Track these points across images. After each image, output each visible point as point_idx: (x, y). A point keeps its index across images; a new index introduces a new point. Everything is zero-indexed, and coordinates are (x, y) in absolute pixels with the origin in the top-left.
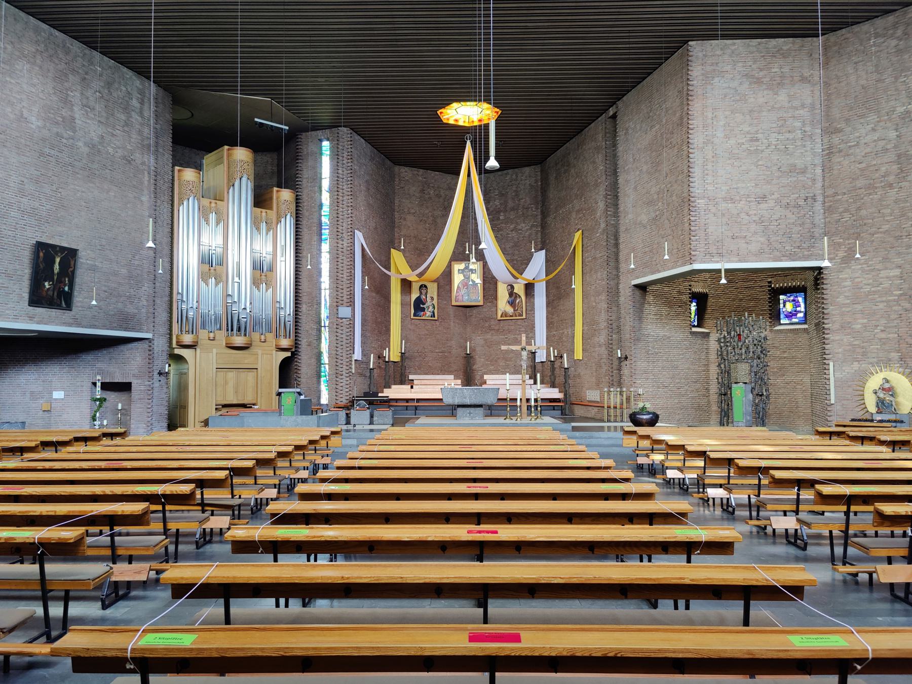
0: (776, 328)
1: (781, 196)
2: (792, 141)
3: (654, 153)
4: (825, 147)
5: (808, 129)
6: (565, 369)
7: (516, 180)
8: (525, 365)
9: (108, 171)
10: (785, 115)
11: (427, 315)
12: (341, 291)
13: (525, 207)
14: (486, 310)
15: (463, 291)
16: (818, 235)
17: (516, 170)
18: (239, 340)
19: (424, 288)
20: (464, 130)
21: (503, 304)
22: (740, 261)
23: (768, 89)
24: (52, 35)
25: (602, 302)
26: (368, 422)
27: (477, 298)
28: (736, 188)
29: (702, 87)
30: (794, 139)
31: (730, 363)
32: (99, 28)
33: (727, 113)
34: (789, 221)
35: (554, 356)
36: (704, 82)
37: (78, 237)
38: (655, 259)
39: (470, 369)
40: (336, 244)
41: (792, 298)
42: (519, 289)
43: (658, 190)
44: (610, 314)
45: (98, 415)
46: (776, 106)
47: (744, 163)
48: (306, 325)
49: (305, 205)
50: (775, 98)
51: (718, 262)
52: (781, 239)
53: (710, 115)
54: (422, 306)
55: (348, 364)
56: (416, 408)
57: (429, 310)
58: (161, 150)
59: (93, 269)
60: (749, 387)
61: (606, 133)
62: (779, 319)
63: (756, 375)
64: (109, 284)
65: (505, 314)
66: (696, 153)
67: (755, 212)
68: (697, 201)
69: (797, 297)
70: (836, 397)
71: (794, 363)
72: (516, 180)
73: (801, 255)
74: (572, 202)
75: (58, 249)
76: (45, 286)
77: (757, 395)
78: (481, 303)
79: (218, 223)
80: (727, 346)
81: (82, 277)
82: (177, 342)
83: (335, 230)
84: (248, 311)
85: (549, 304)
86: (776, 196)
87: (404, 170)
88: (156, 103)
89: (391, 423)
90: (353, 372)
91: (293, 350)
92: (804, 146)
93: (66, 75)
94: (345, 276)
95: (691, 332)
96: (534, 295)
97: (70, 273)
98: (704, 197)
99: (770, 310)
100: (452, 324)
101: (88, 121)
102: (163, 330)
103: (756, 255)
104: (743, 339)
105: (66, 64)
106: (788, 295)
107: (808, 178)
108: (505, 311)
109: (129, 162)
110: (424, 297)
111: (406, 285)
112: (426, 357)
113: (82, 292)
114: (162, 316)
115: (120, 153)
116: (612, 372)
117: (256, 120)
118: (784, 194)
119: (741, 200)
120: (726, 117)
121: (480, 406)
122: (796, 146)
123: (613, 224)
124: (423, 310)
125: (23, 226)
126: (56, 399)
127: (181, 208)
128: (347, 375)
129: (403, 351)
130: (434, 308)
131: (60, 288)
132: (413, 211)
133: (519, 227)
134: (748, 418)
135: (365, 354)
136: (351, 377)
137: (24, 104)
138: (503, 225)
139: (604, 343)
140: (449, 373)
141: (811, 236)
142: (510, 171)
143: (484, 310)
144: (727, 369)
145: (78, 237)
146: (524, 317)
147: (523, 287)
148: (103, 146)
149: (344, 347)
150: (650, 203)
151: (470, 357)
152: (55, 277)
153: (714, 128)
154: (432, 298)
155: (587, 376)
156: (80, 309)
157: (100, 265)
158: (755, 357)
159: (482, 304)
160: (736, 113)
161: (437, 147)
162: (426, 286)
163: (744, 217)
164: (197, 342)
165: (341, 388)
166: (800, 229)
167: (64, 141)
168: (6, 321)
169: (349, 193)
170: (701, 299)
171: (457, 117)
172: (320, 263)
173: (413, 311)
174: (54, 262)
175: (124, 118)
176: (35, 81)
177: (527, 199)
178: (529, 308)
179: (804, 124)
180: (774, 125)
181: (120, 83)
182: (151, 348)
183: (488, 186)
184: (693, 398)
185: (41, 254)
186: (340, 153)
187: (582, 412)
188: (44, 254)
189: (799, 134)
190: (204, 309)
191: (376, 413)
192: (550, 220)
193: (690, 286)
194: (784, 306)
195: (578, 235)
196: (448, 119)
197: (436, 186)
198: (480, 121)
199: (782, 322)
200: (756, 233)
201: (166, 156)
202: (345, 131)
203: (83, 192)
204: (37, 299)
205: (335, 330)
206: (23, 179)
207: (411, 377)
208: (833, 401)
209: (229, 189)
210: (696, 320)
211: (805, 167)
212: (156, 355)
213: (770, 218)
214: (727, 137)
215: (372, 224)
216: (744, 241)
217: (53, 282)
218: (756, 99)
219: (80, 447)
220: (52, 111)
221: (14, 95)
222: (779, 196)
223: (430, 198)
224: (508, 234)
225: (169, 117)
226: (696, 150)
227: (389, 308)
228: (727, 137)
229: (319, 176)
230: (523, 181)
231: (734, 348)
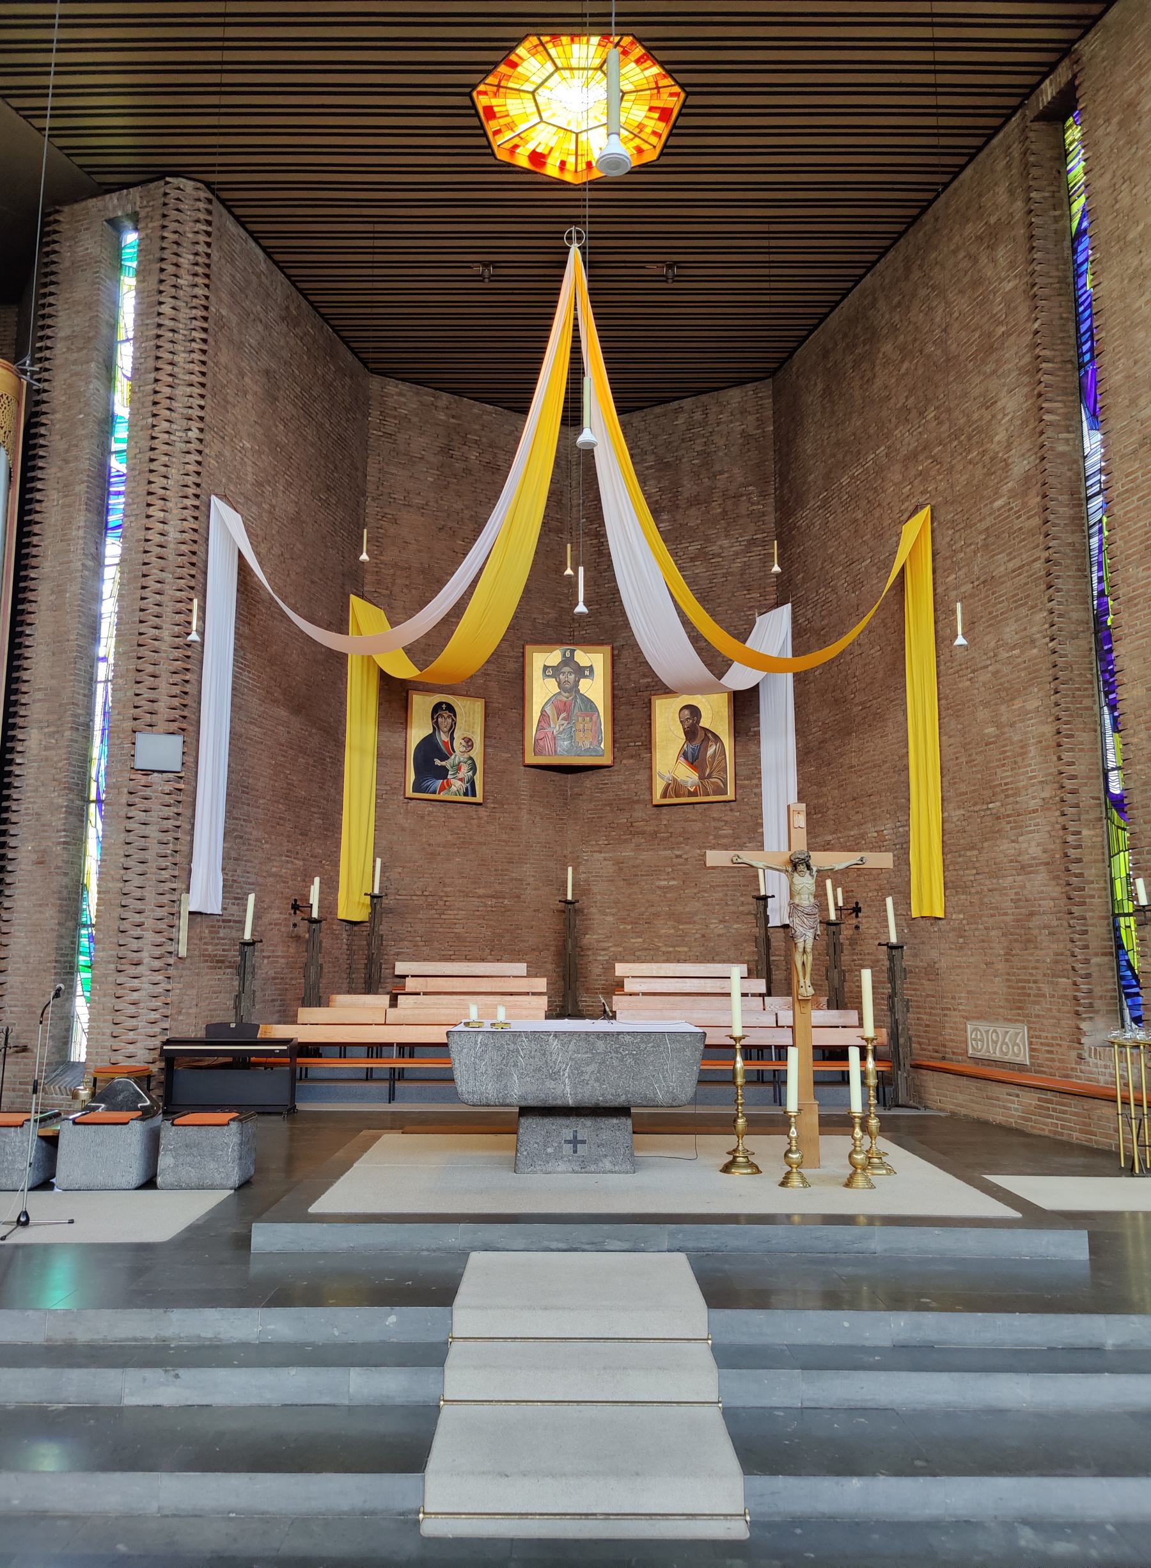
6: (892, 947)
7: (704, 423)
8: (810, 934)
11: (454, 788)
13: (731, 493)
14: (620, 778)
17: (704, 398)
19: (446, 714)
26: (135, 1175)
35: (838, 909)
39: (575, 946)
40: (141, 535)
54: (438, 762)
55: (162, 925)
56: (396, 1076)
57: (460, 775)
61: (1026, 166)
65: (675, 788)
78: (607, 760)
83: (143, 489)
85: (804, 756)
87: (393, 387)
90: (183, 951)
96: (758, 734)
100: (525, 816)
108: (675, 780)
112: (449, 908)
116: (1087, 961)
121: (622, 1111)
123: (1063, 454)
124: (442, 773)
128: (157, 964)
129: (376, 891)
130: (473, 768)
132: (418, 501)
133: (715, 549)
135: (233, 892)
136: (171, 971)
139: (1044, 857)
140: (515, 957)
142: (687, 403)
143: (615, 779)
149: (151, 867)
151: (575, 911)
154: (469, 743)
162: (450, 708)
165: (132, 1010)
169: (196, 379)
172: (97, 598)
173: (411, 776)
177: (736, 471)
187: (961, 1098)
191: (170, 1135)
192: (803, 517)
197: (484, 440)
205: (124, 811)
207: (401, 968)
223: (468, 471)
229: (104, 330)
230: (723, 427)
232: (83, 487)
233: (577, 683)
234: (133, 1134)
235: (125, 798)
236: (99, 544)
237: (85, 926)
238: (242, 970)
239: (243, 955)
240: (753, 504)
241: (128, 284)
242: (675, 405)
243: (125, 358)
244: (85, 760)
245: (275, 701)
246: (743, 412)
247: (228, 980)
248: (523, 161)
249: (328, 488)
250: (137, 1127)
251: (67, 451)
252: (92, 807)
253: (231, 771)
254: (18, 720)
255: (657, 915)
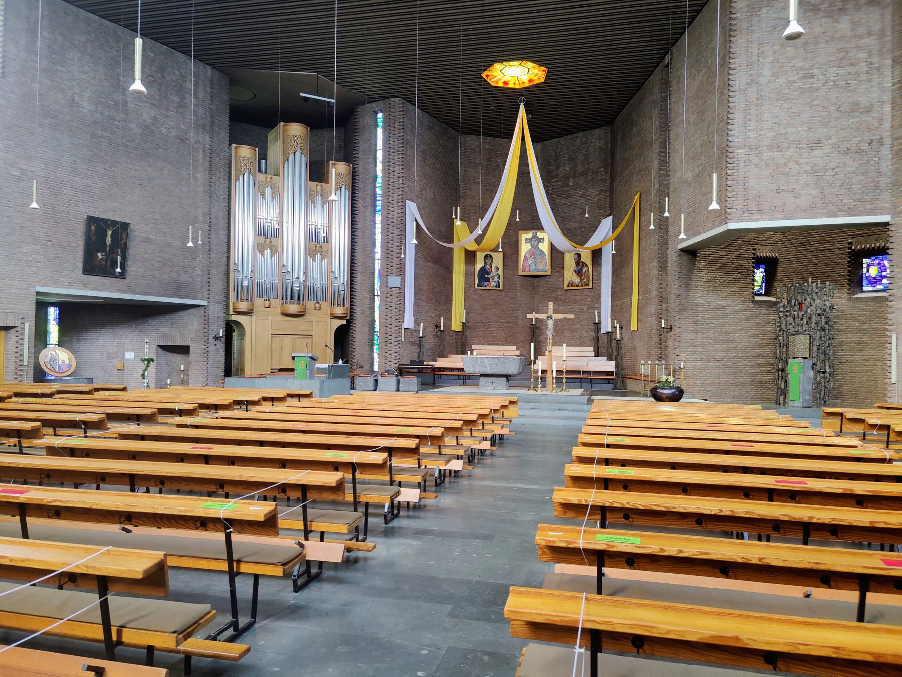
0: (856, 296)
1: (840, 141)
2: (855, 76)
3: (700, 102)
4: (896, 80)
5: (875, 59)
6: (618, 340)
9: (161, 150)
10: (847, 45)
11: (492, 285)
12: (391, 261)
13: (595, 171)
15: (530, 261)
16: (884, 185)
17: (586, 132)
18: (293, 308)
19: (489, 258)
20: (514, 92)
21: (570, 275)
22: (786, 218)
23: (826, 16)
24: (102, 25)
25: (653, 268)
26: (395, 388)
27: (544, 267)
28: (785, 134)
29: (747, 20)
30: (857, 73)
31: (789, 335)
32: (461, 57)
33: (776, 47)
34: (849, 169)
36: (749, 14)
37: (132, 212)
38: (696, 220)
40: (387, 215)
41: (877, 262)
42: (586, 258)
43: (702, 142)
44: (660, 282)
45: (146, 374)
46: (836, 36)
47: (795, 104)
48: (361, 294)
49: (360, 177)
50: (835, 27)
51: (758, 220)
52: (838, 191)
53: (755, 51)
54: (486, 276)
55: (397, 332)
57: (494, 280)
58: (217, 129)
59: (147, 241)
60: (809, 363)
62: (862, 286)
63: (819, 349)
64: (163, 255)
65: (571, 284)
66: (737, 96)
67: (806, 160)
68: (737, 151)
69: (883, 260)
70: (898, 375)
71: (875, 337)
72: (586, 143)
73: (862, 208)
74: (634, 163)
75: (109, 222)
76: (98, 257)
77: (819, 372)
78: (548, 273)
79: (273, 198)
80: (787, 316)
81: (135, 248)
82: (234, 309)
84: (302, 281)
86: (834, 140)
88: (211, 84)
89: (416, 390)
90: (403, 340)
91: (348, 318)
92: (870, 81)
93: (118, 62)
94: (395, 246)
95: (753, 302)
97: (123, 245)
98: (745, 147)
99: (849, 276)
100: (518, 294)
101: (140, 104)
102: (220, 297)
103: (805, 211)
104: (804, 308)
105: (117, 51)
106: (873, 258)
107: (874, 118)
108: (571, 281)
109: (184, 141)
110: (488, 267)
111: (470, 256)
113: (136, 262)
114: (218, 285)
115: (174, 133)
116: (661, 344)
117: (302, 94)
118: (843, 138)
119: (790, 148)
120: (775, 52)
122: (860, 81)
124: (488, 280)
125: (75, 202)
126: (128, 359)
127: (237, 183)
128: (396, 343)
129: (464, 321)
130: (499, 278)
131: (113, 259)
133: (588, 193)
134: (807, 397)
135: (417, 323)
136: (400, 345)
137: (76, 90)
138: (572, 191)
141: (875, 186)
142: (580, 134)
143: (552, 280)
144: (785, 342)
145: (132, 212)
146: (590, 286)
147: (590, 256)
148: (156, 127)
150: (694, 158)
152: (108, 249)
153: (760, 66)
154: (497, 268)
155: (641, 346)
156: (134, 277)
157: (154, 238)
158: (819, 328)
159: (549, 274)
160: (787, 46)
161: (493, 113)
162: (490, 256)
163: (792, 167)
164: (252, 310)
165: (390, 356)
166: (863, 178)
167: (117, 123)
168: (60, 288)
170: (771, 265)
171: (505, 79)
172: (374, 234)
173: (477, 281)
174: (106, 235)
175: (178, 100)
176: (86, 68)
178: (595, 278)
179: (870, 54)
180: (834, 58)
181: (173, 67)
182: (206, 314)
183: (558, 151)
184: (753, 374)
185: (93, 228)
186: (391, 124)
188: (96, 227)
189: (864, 67)
190: (258, 279)
192: (616, 184)
193: (754, 250)
194: (868, 271)
195: (637, 197)
196: (497, 82)
198: (530, 81)
199: (865, 289)
200: (806, 185)
201: (223, 134)
202: (397, 101)
203: (137, 170)
204: (90, 267)
206: (75, 159)
208: (894, 380)
209: (284, 164)
210: (763, 288)
211: (871, 105)
212: (211, 321)
213: (824, 167)
214: (776, 75)
215: (429, 194)
216: (792, 195)
217: (106, 254)
218: (812, 29)
219: (267, 407)
220: (104, 96)
221: (65, 82)
222: (837, 140)
224: (577, 200)
225: (226, 97)
226: (737, 93)
227: (451, 278)
228: (776, 75)
229: (373, 148)
230: (593, 144)
231: (794, 319)
232: (369, 200)
233: (538, 244)
234: (394, 379)
235: (385, 296)
236: (374, 216)
237: (376, 332)
238: (420, 346)
239: (420, 341)
240: (602, 175)
241: (380, 131)
242: (575, 135)
243: (380, 155)
244: (374, 284)
245: (428, 261)
246: (600, 139)
247: (415, 349)
248: (501, 85)
249: (445, 183)
250: (395, 377)
251: (364, 187)
252: (376, 297)
253: (415, 285)
254: (354, 272)
255: (564, 329)
